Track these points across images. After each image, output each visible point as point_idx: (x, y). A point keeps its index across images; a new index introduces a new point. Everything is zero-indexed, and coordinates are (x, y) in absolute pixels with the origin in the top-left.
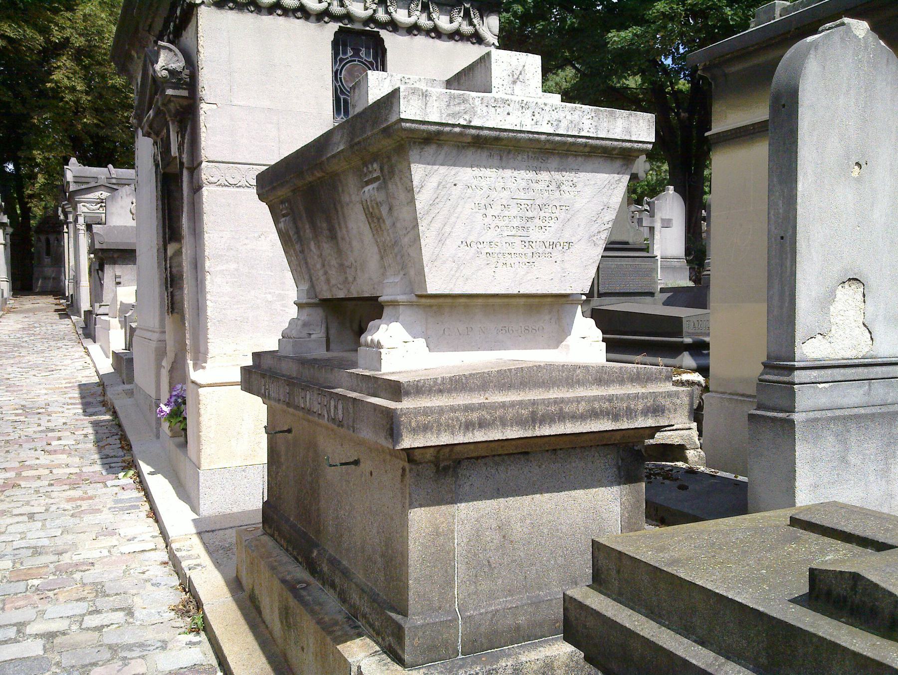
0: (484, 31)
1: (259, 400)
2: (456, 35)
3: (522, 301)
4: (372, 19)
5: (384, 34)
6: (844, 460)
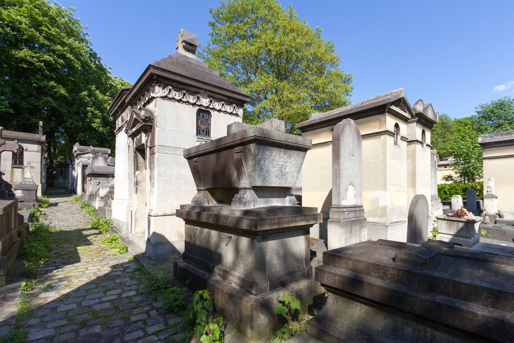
0: (239, 113)
1: (376, 240)
2: (231, 114)
3: (277, 189)
4: (208, 107)
5: (211, 111)
6: (351, 232)
